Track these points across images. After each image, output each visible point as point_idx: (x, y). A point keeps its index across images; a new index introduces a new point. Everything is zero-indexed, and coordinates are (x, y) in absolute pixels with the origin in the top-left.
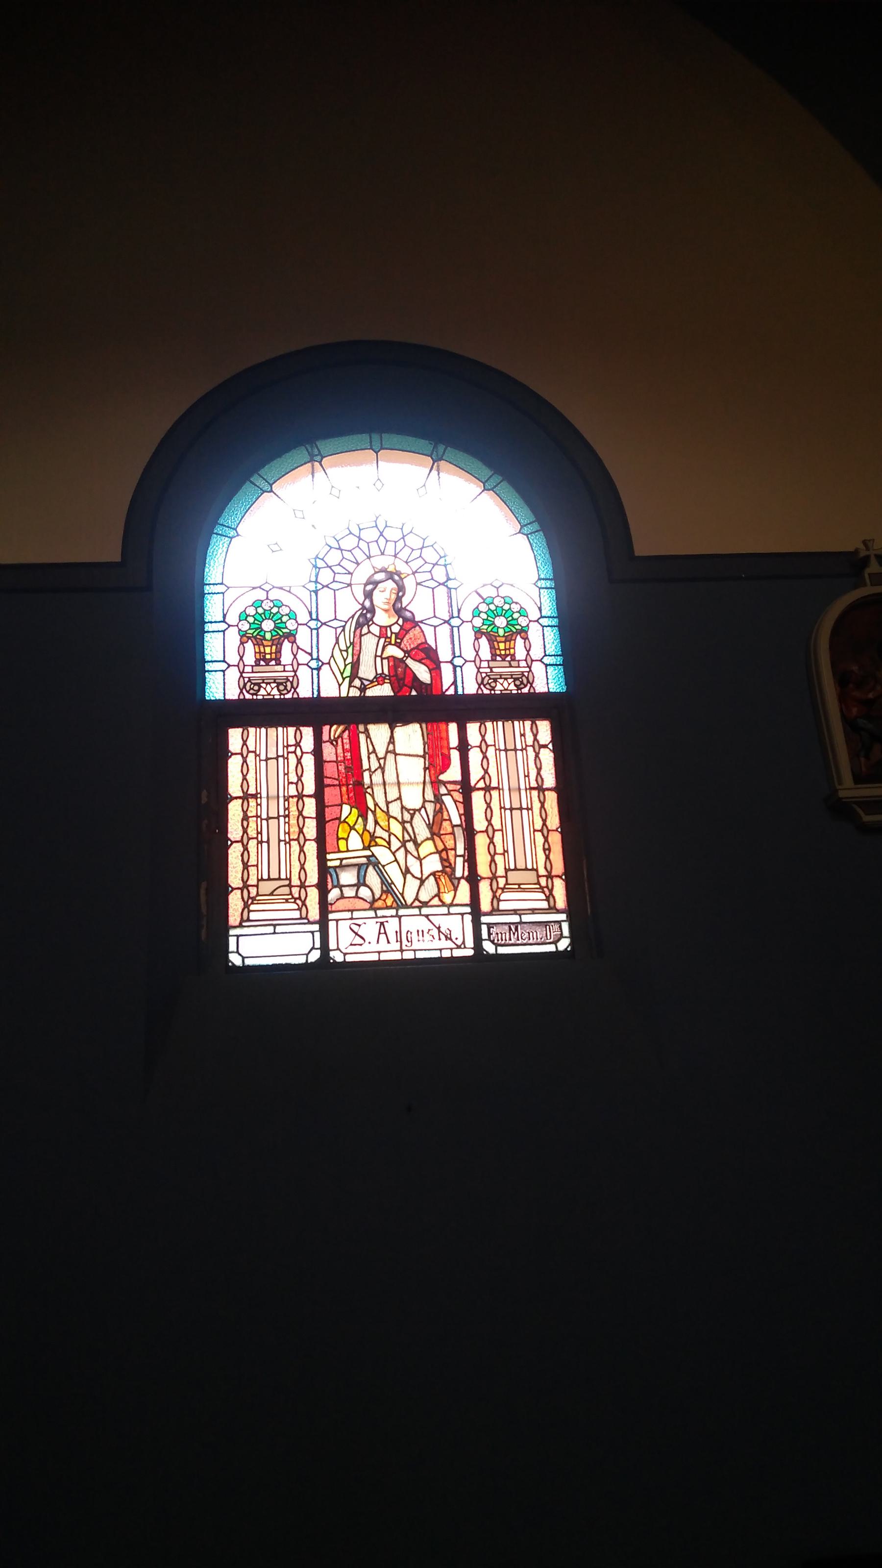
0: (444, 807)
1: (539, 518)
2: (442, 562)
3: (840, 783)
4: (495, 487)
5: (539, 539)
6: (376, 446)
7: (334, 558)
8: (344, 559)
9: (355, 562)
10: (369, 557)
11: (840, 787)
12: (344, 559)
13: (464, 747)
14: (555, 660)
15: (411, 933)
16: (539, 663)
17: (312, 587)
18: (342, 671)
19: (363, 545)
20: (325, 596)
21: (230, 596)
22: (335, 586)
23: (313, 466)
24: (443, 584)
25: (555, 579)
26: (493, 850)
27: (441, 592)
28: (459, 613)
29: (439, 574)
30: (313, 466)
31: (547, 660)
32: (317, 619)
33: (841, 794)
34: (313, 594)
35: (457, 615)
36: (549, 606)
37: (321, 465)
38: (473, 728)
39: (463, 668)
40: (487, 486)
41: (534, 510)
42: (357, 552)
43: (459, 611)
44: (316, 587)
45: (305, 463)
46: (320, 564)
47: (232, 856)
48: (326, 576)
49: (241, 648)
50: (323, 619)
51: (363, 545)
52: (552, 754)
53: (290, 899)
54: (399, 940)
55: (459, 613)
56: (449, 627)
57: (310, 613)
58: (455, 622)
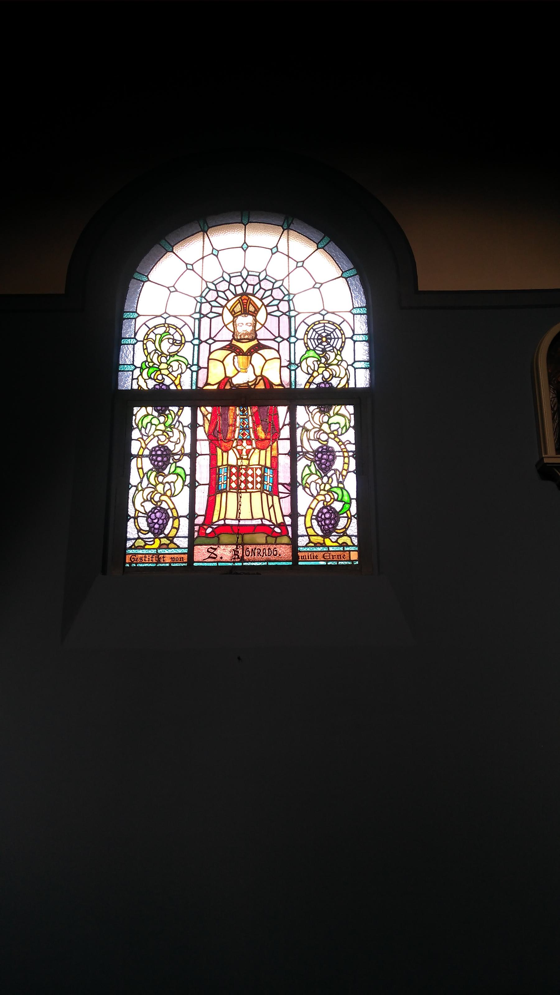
1: (356, 266)
2: (286, 298)
3: (546, 453)
5: (356, 281)
8: (222, 360)
9: (226, 298)
12: (222, 360)
13: (293, 425)
15: (241, 326)
16: (350, 340)
17: (197, 316)
18: (211, 351)
19: (232, 288)
20: (205, 321)
21: (140, 321)
22: (211, 315)
24: (287, 339)
26: (311, 456)
27: (284, 319)
29: (284, 307)
35: (294, 335)
38: (300, 410)
39: (298, 261)
40: (320, 246)
42: (228, 293)
43: (296, 331)
44: (200, 317)
45: (198, 232)
47: (129, 543)
48: (206, 308)
50: (203, 338)
51: (232, 288)
52: (355, 475)
56: (288, 343)
57: (193, 334)
58: (293, 340)
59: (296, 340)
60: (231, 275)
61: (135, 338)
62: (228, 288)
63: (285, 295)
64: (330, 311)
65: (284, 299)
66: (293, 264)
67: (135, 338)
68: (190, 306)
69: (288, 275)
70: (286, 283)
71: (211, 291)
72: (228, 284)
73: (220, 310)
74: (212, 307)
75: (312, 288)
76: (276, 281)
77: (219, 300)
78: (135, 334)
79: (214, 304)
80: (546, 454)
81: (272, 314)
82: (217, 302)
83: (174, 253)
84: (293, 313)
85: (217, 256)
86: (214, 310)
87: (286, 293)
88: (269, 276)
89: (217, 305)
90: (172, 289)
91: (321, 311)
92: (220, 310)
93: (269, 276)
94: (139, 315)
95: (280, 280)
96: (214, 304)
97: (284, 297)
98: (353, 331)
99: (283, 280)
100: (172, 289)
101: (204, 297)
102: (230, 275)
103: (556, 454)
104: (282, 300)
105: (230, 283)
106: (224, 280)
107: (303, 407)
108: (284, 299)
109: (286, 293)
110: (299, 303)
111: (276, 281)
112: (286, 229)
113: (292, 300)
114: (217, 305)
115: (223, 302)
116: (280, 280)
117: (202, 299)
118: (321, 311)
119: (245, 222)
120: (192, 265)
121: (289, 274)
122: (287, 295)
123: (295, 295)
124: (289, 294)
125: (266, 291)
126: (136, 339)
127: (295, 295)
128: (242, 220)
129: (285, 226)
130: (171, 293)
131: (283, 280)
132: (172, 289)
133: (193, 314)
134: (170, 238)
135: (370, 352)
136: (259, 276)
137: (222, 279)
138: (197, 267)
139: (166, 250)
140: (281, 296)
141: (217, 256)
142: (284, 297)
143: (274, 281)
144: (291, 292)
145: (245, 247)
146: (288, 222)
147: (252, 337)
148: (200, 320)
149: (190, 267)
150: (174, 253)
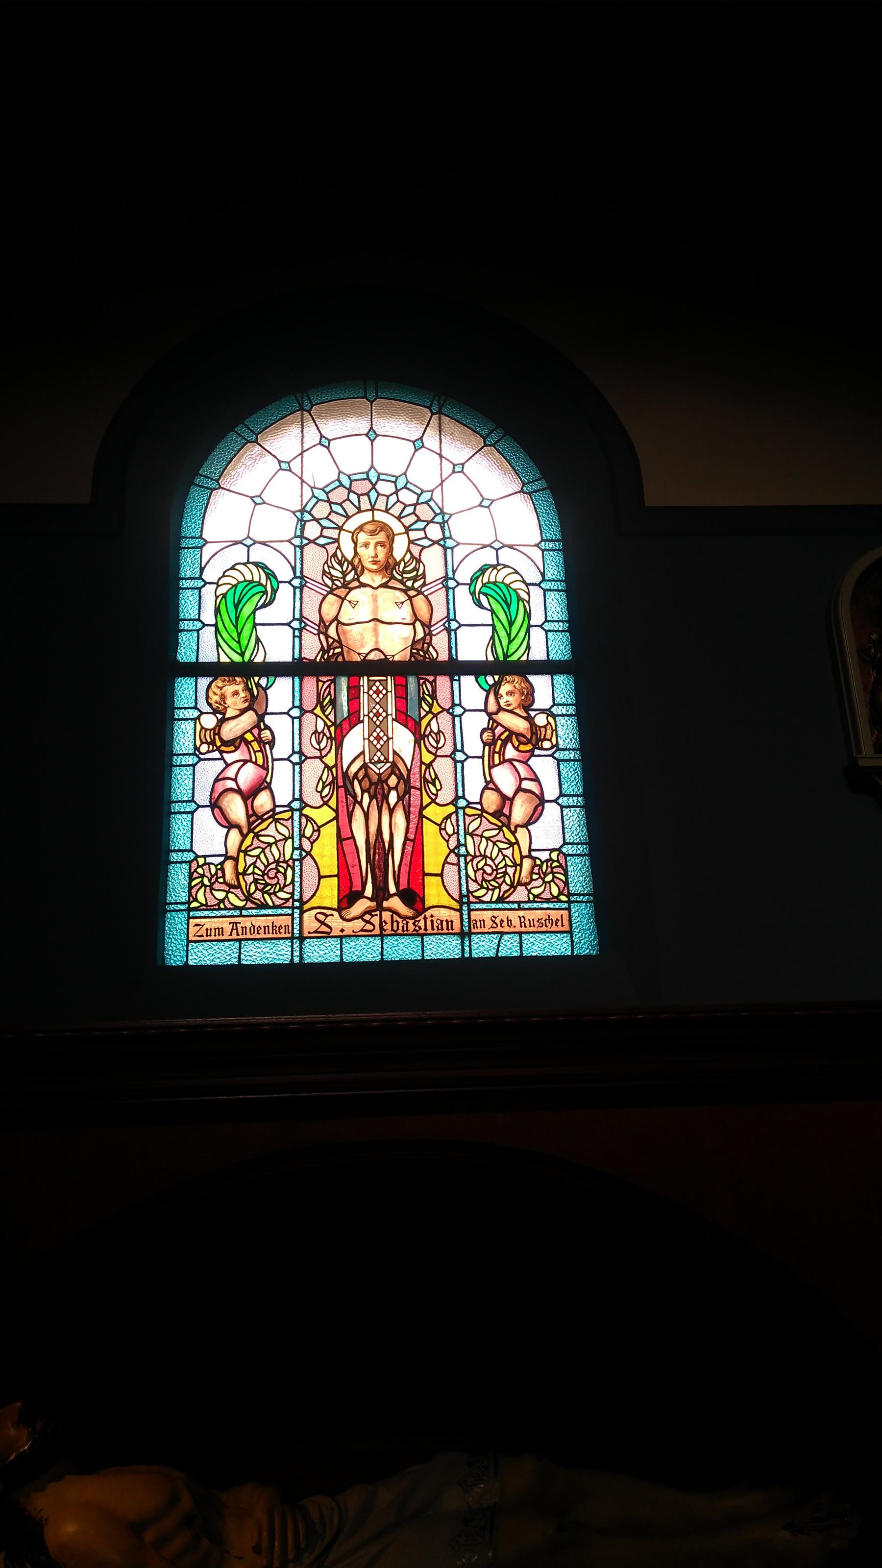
0: (473, 578)
2: (439, 519)
3: (859, 751)
4: (496, 442)
5: (546, 499)
6: (372, 395)
7: (321, 510)
10: (340, 528)
11: (860, 756)
14: (557, 626)
17: (297, 542)
21: (208, 551)
23: (302, 415)
25: (563, 540)
28: (454, 575)
29: (434, 532)
30: (302, 415)
31: (547, 626)
32: (405, 487)
33: (862, 763)
34: (298, 549)
36: (555, 570)
37: (311, 415)
41: (563, 531)
42: (347, 505)
43: (454, 572)
44: (301, 543)
46: (307, 517)
49: (242, 585)
53: (260, 880)
54: (509, 922)
55: (454, 575)
57: (294, 569)
59: (456, 584)
60: (353, 478)
61: (200, 578)
62: (346, 498)
63: (436, 515)
64: (506, 543)
65: (435, 520)
66: (448, 468)
67: (200, 578)
68: (287, 526)
69: (442, 482)
70: (437, 496)
71: (320, 503)
72: (347, 491)
73: (334, 534)
74: (323, 528)
75: (477, 507)
76: (423, 491)
77: (333, 517)
78: (202, 570)
79: (325, 523)
80: (860, 754)
81: (417, 542)
82: (331, 521)
83: (223, 488)
84: (450, 543)
85: (328, 448)
86: (333, 517)
87: (438, 511)
88: (411, 484)
89: (342, 512)
90: (258, 500)
91: (492, 543)
92: (334, 534)
93: (411, 484)
94: (206, 542)
95: (428, 491)
96: (325, 523)
97: (434, 518)
98: (543, 574)
99: (432, 491)
100: (257, 500)
101: (309, 513)
102: (351, 476)
103: (875, 754)
104: (432, 521)
105: (350, 490)
106: (341, 485)
107: (472, 678)
108: (435, 520)
109: (438, 511)
110: (458, 528)
111: (423, 491)
112: (435, 414)
113: (447, 522)
114: (342, 512)
115: (340, 521)
116: (428, 491)
117: (302, 516)
118: (492, 543)
119: (372, 395)
120: (260, 496)
121: (442, 482)
122: (439, 514)
123: (451, 515)
124: (442, 513)
125: (406, 506)
126: (203, 580)
127: (451, 515)
128: (366, 394)
129: (435, 408)
130: (257, 506)
131: (432, 491)
132: (257, 500)
133: (292, 539)
134: (209, 468)
135: (571, 607)
136: (395, 482)
137: (337, 484)
138: (296, 466)
139: (207, 488)
140: (429, 515)
141: (328, 448)
142: (434, 518)
143: (419, 492)
144: (445, 510)
145: (372, 435)
146: (439, 402)
147: (185, 900)
148: (302, 547)
149: (284, 466)
150: (223, 488)
